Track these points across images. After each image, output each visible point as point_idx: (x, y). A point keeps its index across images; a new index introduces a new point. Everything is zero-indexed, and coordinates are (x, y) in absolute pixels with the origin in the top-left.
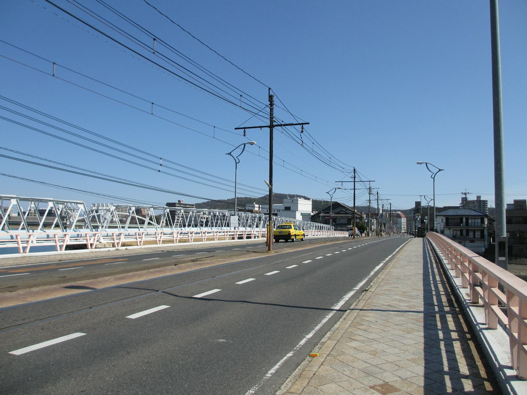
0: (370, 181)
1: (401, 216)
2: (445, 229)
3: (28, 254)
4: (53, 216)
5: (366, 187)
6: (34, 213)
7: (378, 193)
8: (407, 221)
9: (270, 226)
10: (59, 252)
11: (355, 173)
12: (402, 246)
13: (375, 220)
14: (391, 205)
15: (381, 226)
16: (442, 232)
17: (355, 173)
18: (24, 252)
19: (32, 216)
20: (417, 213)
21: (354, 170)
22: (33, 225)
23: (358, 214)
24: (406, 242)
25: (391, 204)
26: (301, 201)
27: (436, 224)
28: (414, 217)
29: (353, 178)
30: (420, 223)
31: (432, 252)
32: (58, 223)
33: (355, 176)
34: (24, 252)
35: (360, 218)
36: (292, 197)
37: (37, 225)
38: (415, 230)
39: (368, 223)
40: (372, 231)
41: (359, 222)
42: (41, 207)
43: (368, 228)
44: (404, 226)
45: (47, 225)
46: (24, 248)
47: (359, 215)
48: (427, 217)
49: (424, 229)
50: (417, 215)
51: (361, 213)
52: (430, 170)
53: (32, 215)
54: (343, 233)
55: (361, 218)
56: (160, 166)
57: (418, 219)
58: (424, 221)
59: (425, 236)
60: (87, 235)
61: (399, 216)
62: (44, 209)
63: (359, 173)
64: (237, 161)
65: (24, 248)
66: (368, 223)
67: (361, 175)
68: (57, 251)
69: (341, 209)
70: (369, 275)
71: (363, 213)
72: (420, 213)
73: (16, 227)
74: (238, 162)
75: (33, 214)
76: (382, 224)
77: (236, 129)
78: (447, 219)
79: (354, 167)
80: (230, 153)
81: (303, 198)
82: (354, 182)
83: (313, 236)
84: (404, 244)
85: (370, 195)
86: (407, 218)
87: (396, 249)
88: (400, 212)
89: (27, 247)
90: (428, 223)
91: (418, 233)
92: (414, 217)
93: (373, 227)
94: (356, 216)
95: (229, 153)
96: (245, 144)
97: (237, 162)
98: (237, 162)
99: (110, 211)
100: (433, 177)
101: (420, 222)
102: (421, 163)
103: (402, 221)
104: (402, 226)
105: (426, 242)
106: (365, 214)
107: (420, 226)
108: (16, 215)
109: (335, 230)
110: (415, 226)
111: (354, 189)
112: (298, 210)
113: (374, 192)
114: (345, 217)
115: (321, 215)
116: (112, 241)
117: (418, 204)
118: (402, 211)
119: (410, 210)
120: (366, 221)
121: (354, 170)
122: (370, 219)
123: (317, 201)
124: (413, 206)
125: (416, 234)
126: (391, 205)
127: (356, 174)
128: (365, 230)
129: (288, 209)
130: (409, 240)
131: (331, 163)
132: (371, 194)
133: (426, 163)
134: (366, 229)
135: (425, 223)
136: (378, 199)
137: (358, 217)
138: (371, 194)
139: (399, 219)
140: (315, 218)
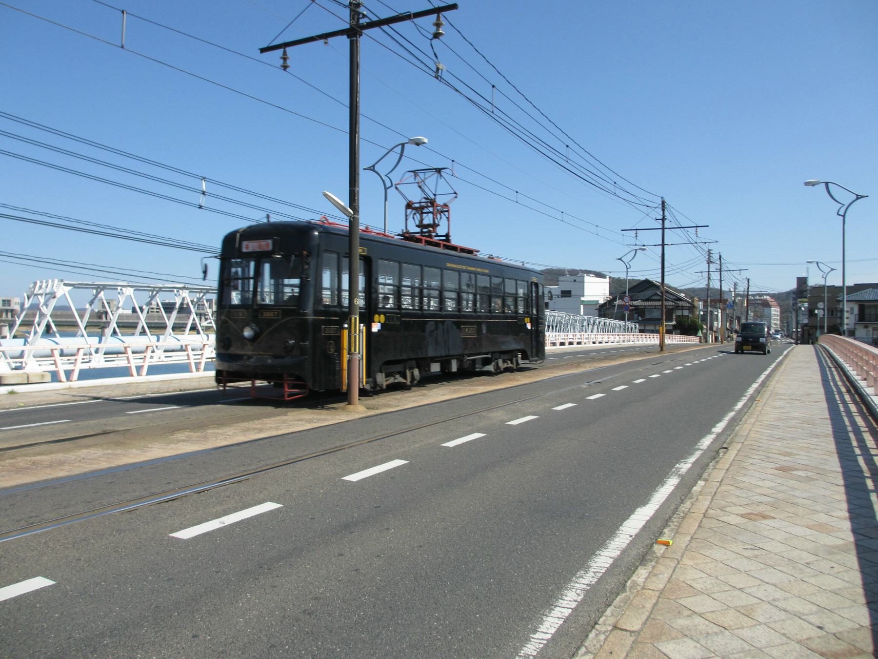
0: (697, 227)
1: (770, 303)
2: (857, 327)
3: (76, 384)
4: (185, 313)
5: (689, 238)
6: (157, 309)
7: (720, 257)
8: (782, 312)
9: (350, 332)
10: (135, 379)
11: (663, 210)
12: (767, 373)
13: (720, 311)
14: (748, 282)
15: (731, 322)
16: (852, 334)
17: (663, 210)
18: (68, 379)
19: (153, 313)
20: (801, 298)
21: (663, 203)
22: (157, 327)
23: (686, 301)
24: (779, 360)
25: (748, 280)
26: (589, 280)
27: (847, 318)
28: (795, 304)
29: (661, 221)
30: (807, 317)
31: (837, 370)
32: (196, 324)
33: (664, 217)
34: (68, 379)
35: (689, 307)
36: (574, 273)
37: (163, 327)
38: (797, 328)
39: (704, 319)
40: (715, 332)
41: (688, 316)
42: (169, 298)
43: (705, 327)
44: (776, 322)
45: (178, 328)
46: (68, 374)
47: (688, 302)
48: (822, 303)
49: (816, 328)
50: (800, 302)
51: (692, 298)
52: (833, 195)
53: (153, 312)
54: (651, 337)
55: (692, 308)
56: (202, 195)
57: (803, 309)
58: (814, 311)
59: (817, 340)
60: (188, 346)
61: (766, 304)
62: (171, 301)
63: (674, 211)
64: (388, 184)
65: (139, 369)
66: (704, 319)
67: (679, 213)
68: (132, 376)
69: (654, 292)
70: (587, 569)
71: (695, 299)
72: (806, 297)
73: (130, 331)
74: (390, 185)
75: (155, 310)
76: (733, 318)
77: (263, 50)
78: (862, 308)
79: (662, 198)
80: (373, 166)
81: (593, 275)
82: (663, 229)
83: (606, 343)
84: (773, 366)
85: (709, 265)
86: (781, 306)
87: (750, 385)
88: (768, 297)
89: (73, 370)
90: (824, 315)
91: (803, 335)
92: (795, 304)
93: (715, 323)
94: (680, 303)
95: (370, 167)
96: (403, 145)
97: (387, 186)
98: (387, 186)
99: (54, 297)
100: (842, 213)
101: (807, 313)
102: (813, 184)
103: (773, 313)
104: (773, 322)
105: (826, 362)
106: (700, 300)
107: (806, 321)
108: (130, 312)
109: (641, 331)
110: (797, 323)
111: (663, 245)
112: (585, 294)
113: (715, 257)
114: (652, 306)
115: (617, 302)
116: (53, 368)
117: (802, 281)
118: (772, 296)
119: (788, 293)
120: (702, 313)
121: (663, 203)
122: (709, 309)
123: (621, 280)
124: (793, 285)
125: (799, 336)
126: (748, 282)
127: (666, 212)
128: (698, 330)
129: (566, 294)
130: (785, 353)
131: (496, 111)
132: (712, 262)
133: (827, 184)
134: (702, 329)
135: (816, 315)
136: (721, 269)
137: (687, 307)
138: (712, 262)
139: (766, 309)
140: (605, 310)
